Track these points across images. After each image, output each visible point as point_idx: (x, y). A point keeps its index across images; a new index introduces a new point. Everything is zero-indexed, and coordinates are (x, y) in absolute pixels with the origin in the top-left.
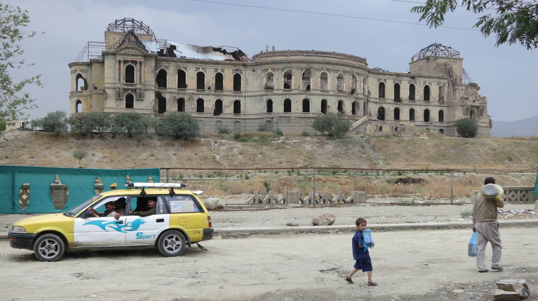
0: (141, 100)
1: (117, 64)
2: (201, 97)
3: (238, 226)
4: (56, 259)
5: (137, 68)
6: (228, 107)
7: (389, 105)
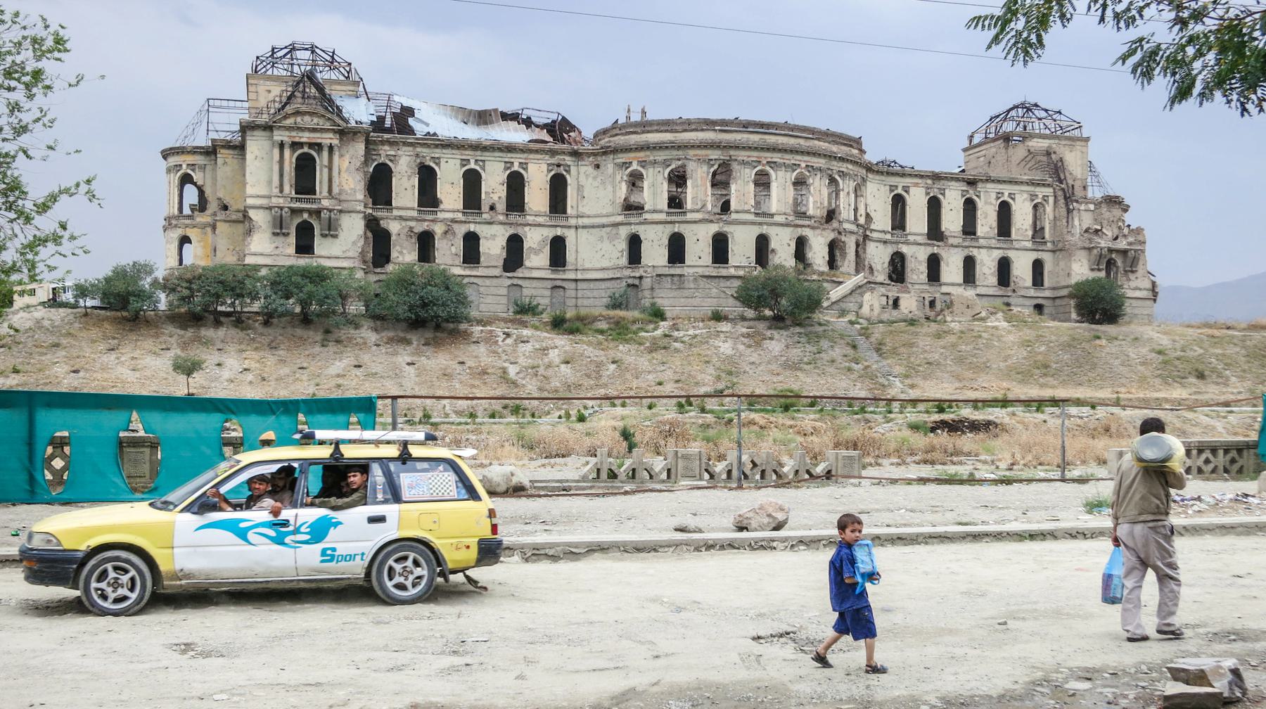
0: (333, 236)
1: (276, 152)
2: (472, 228)
5: (321, 161)
7: (914, 248)
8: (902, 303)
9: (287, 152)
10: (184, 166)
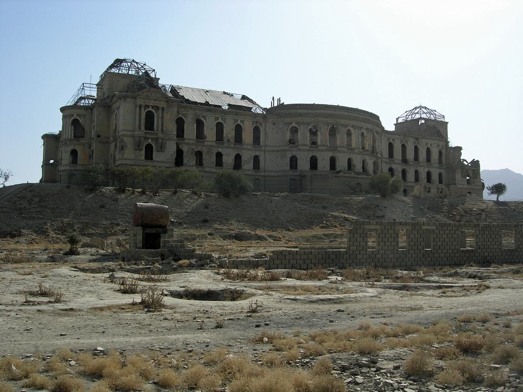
0: (162, 151)
1: (138, 109)
2: (294, 153)
3: (299, 279)
5: (158, 115)
7: (397, 166)
8: (432, 190)
10: (75, 115)
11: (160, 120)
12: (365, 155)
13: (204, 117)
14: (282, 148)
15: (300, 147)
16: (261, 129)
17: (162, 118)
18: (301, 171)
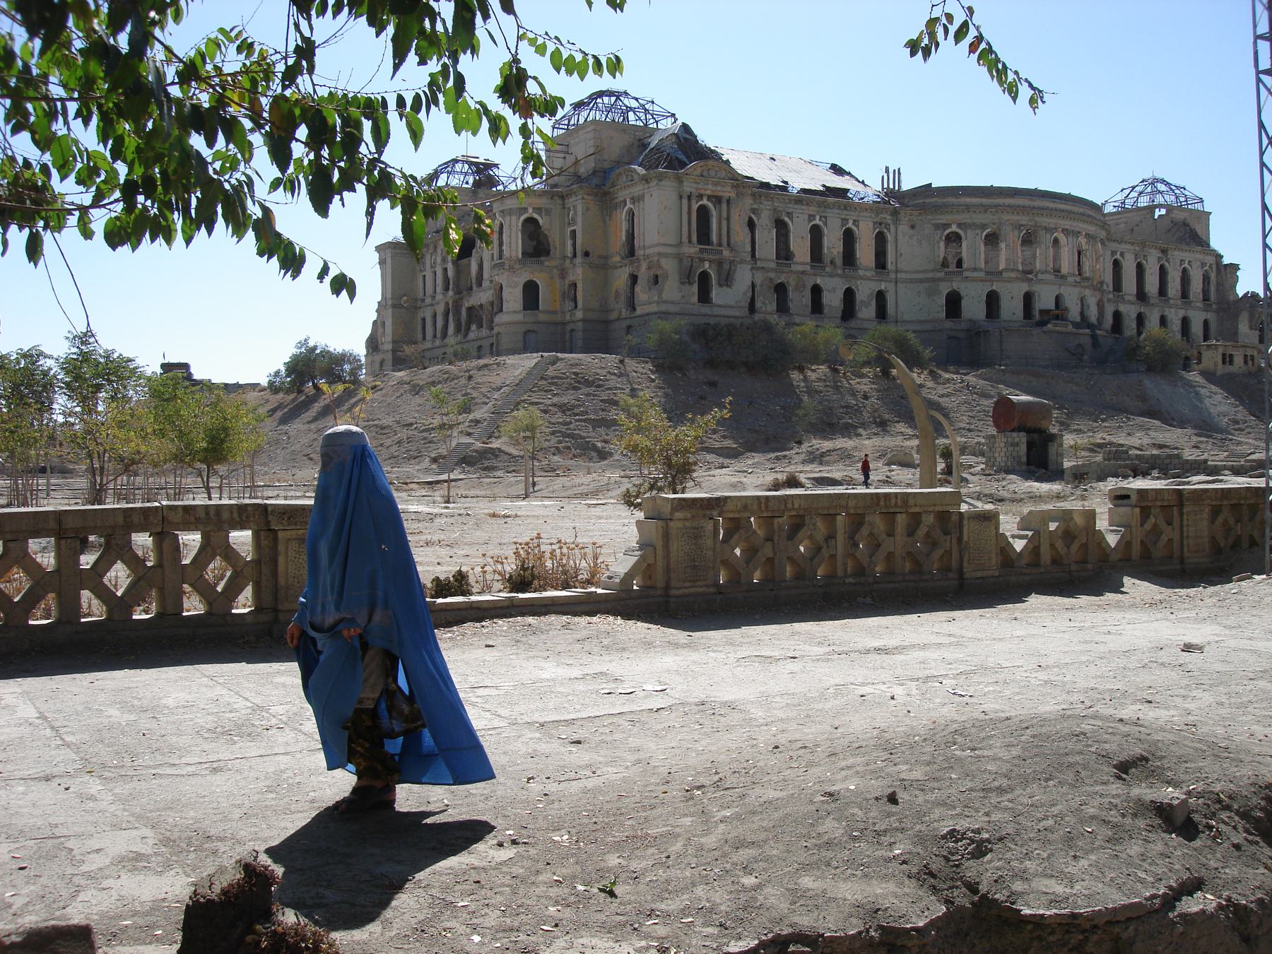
1: (685, 202)
2: (955, 286)
4: (582, 608)
6: (867, 305)
9: (693, 202)
10: (530, 210)
11: (724, 223)
12: (1085, 287)
13: (789, 215)
14: (930, 275)
15: (966, 274)
16: (889, 237)
17: (728, 219)
18: (971, 320)
